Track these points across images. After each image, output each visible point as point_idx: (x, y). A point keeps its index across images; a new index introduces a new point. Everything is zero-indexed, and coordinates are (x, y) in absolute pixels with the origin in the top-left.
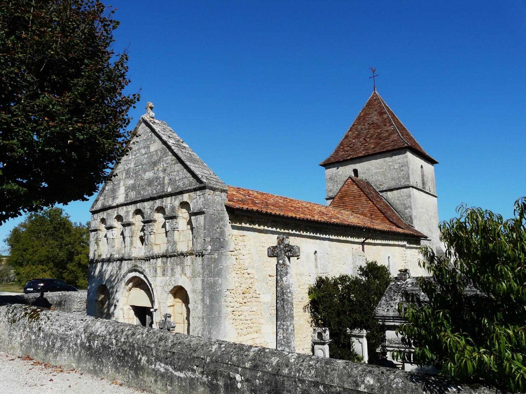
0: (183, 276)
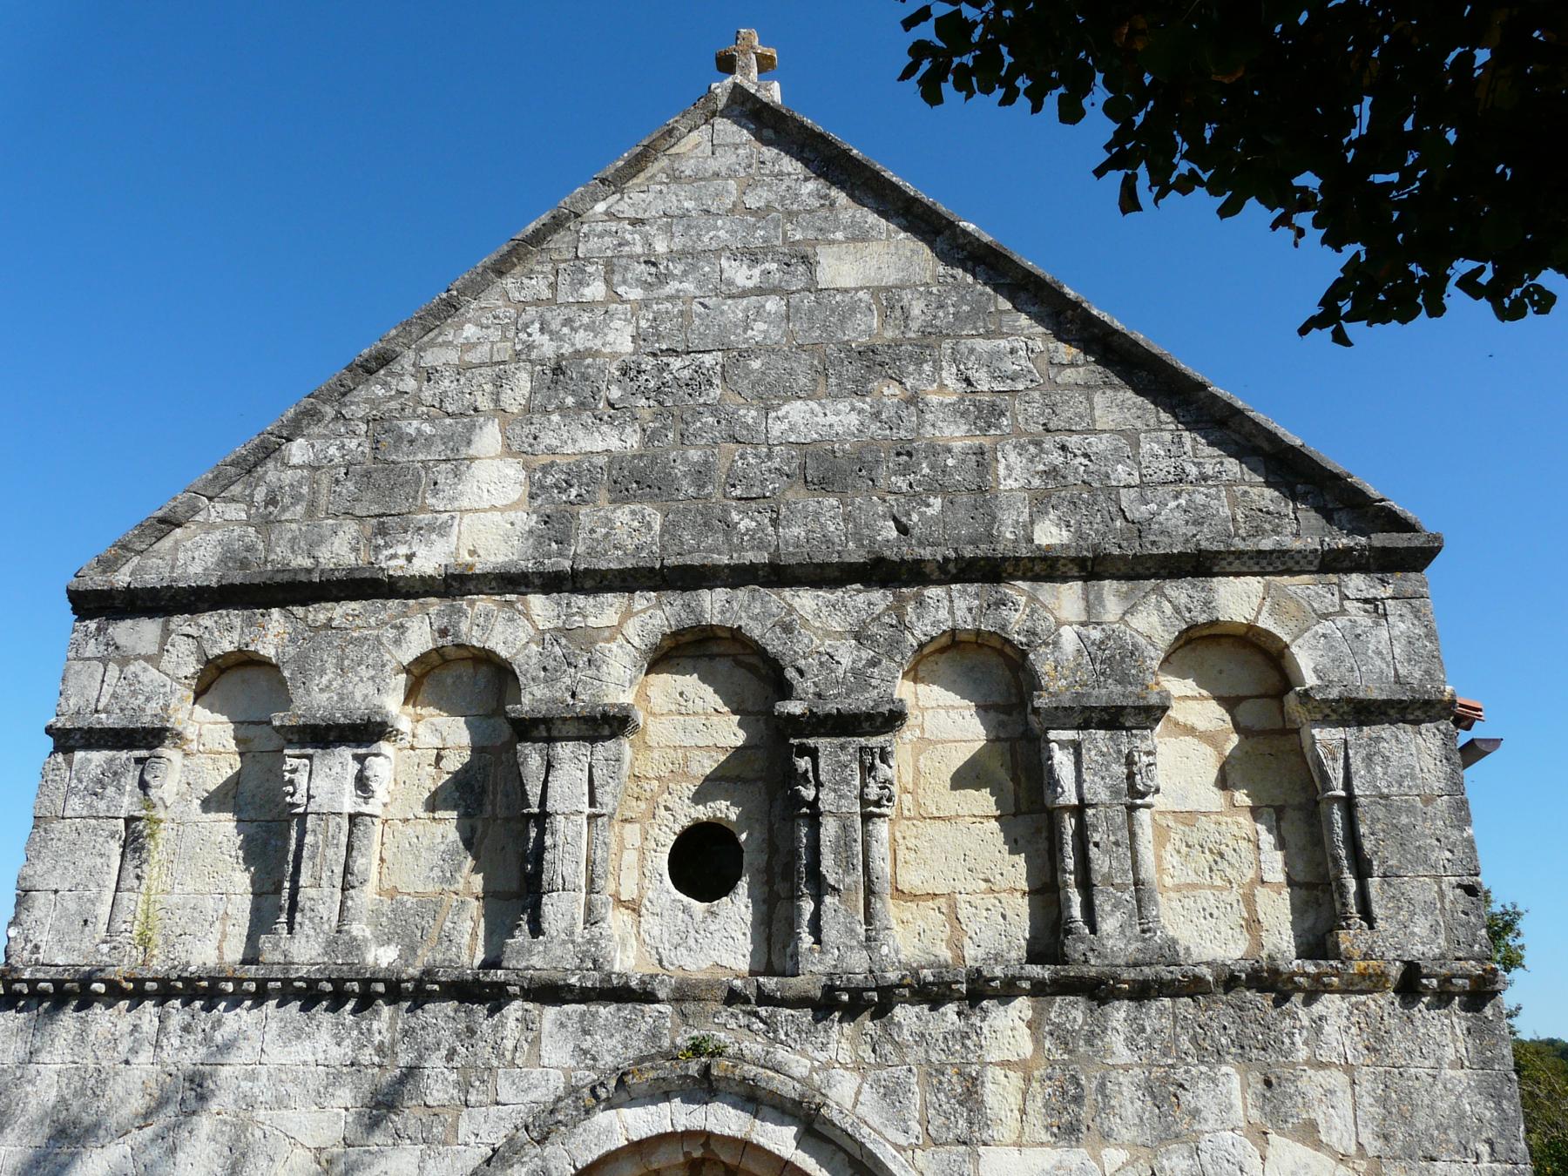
0: (1284, 1150)
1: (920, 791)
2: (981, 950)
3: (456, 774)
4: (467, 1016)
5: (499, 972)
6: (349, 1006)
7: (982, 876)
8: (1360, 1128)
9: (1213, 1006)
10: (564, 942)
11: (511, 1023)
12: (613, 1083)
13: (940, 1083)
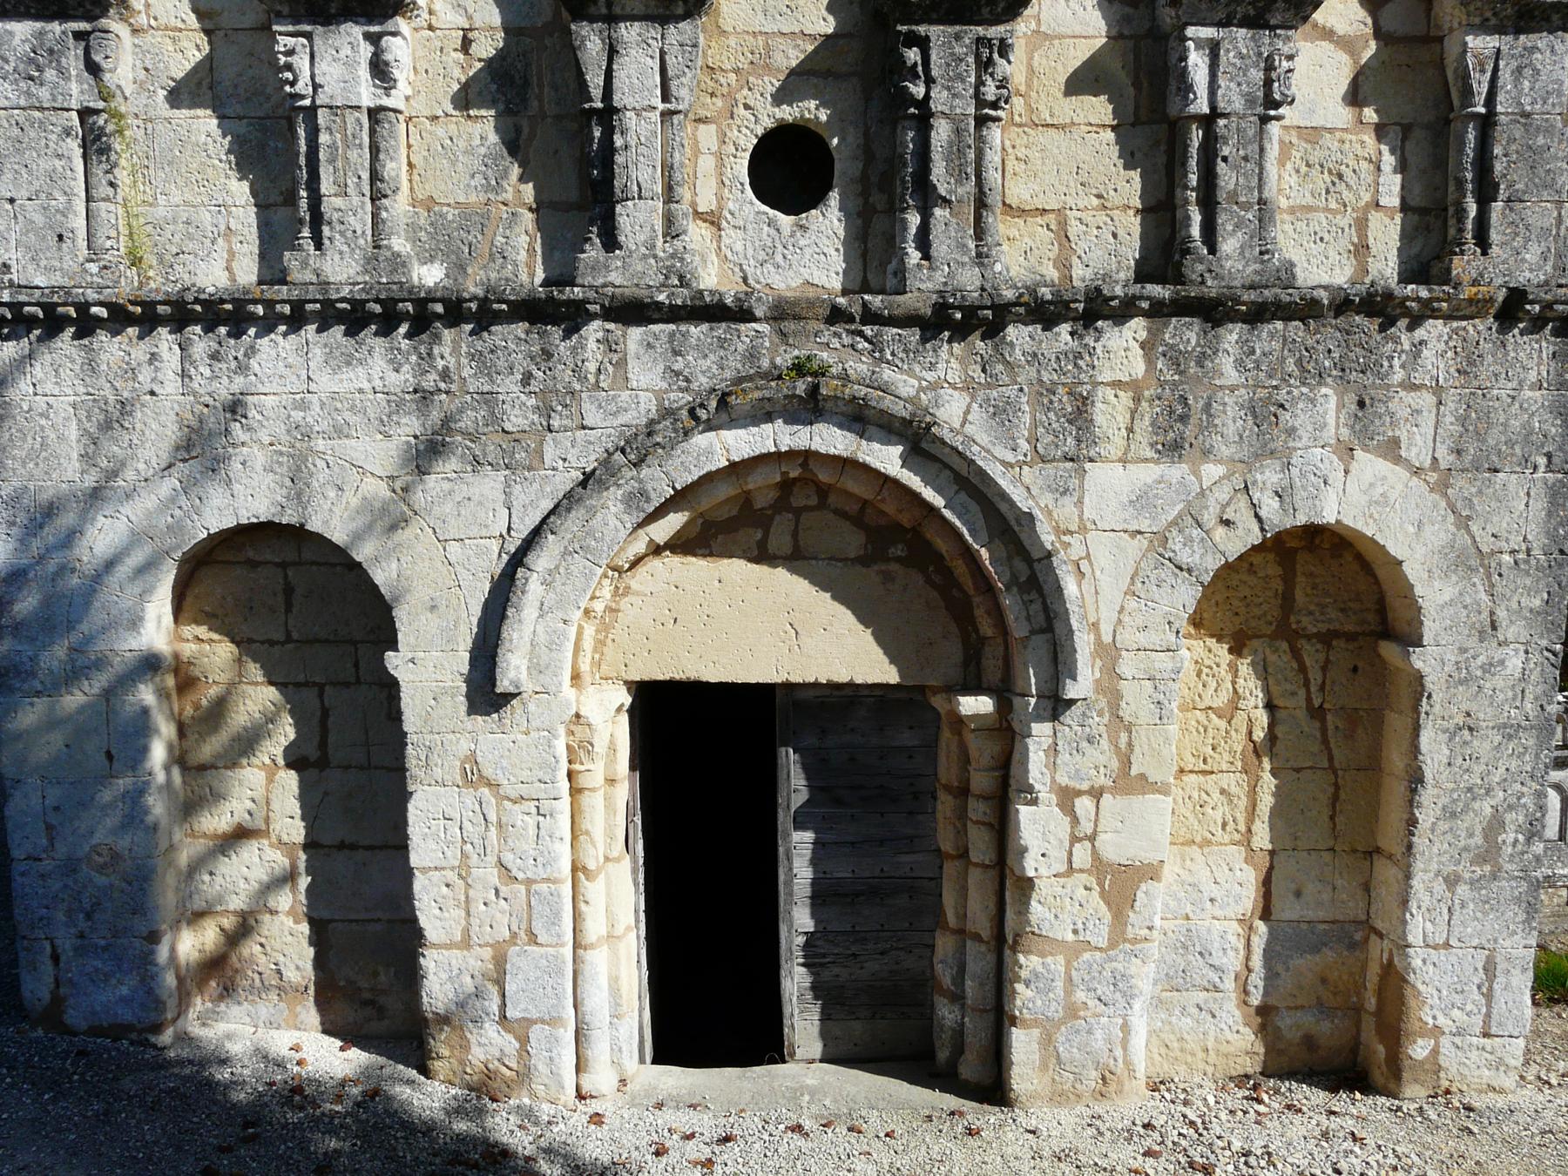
1: (1033, 94)
2: (1090, 270)
3: (489, 62)
6: (403, 329)
7: (1094, 191)
8: (1438, 444)
9: (1322, 329)
10: (645, 257)
11: (592, 345)
12: (714, 404)
13: (1051, 402)
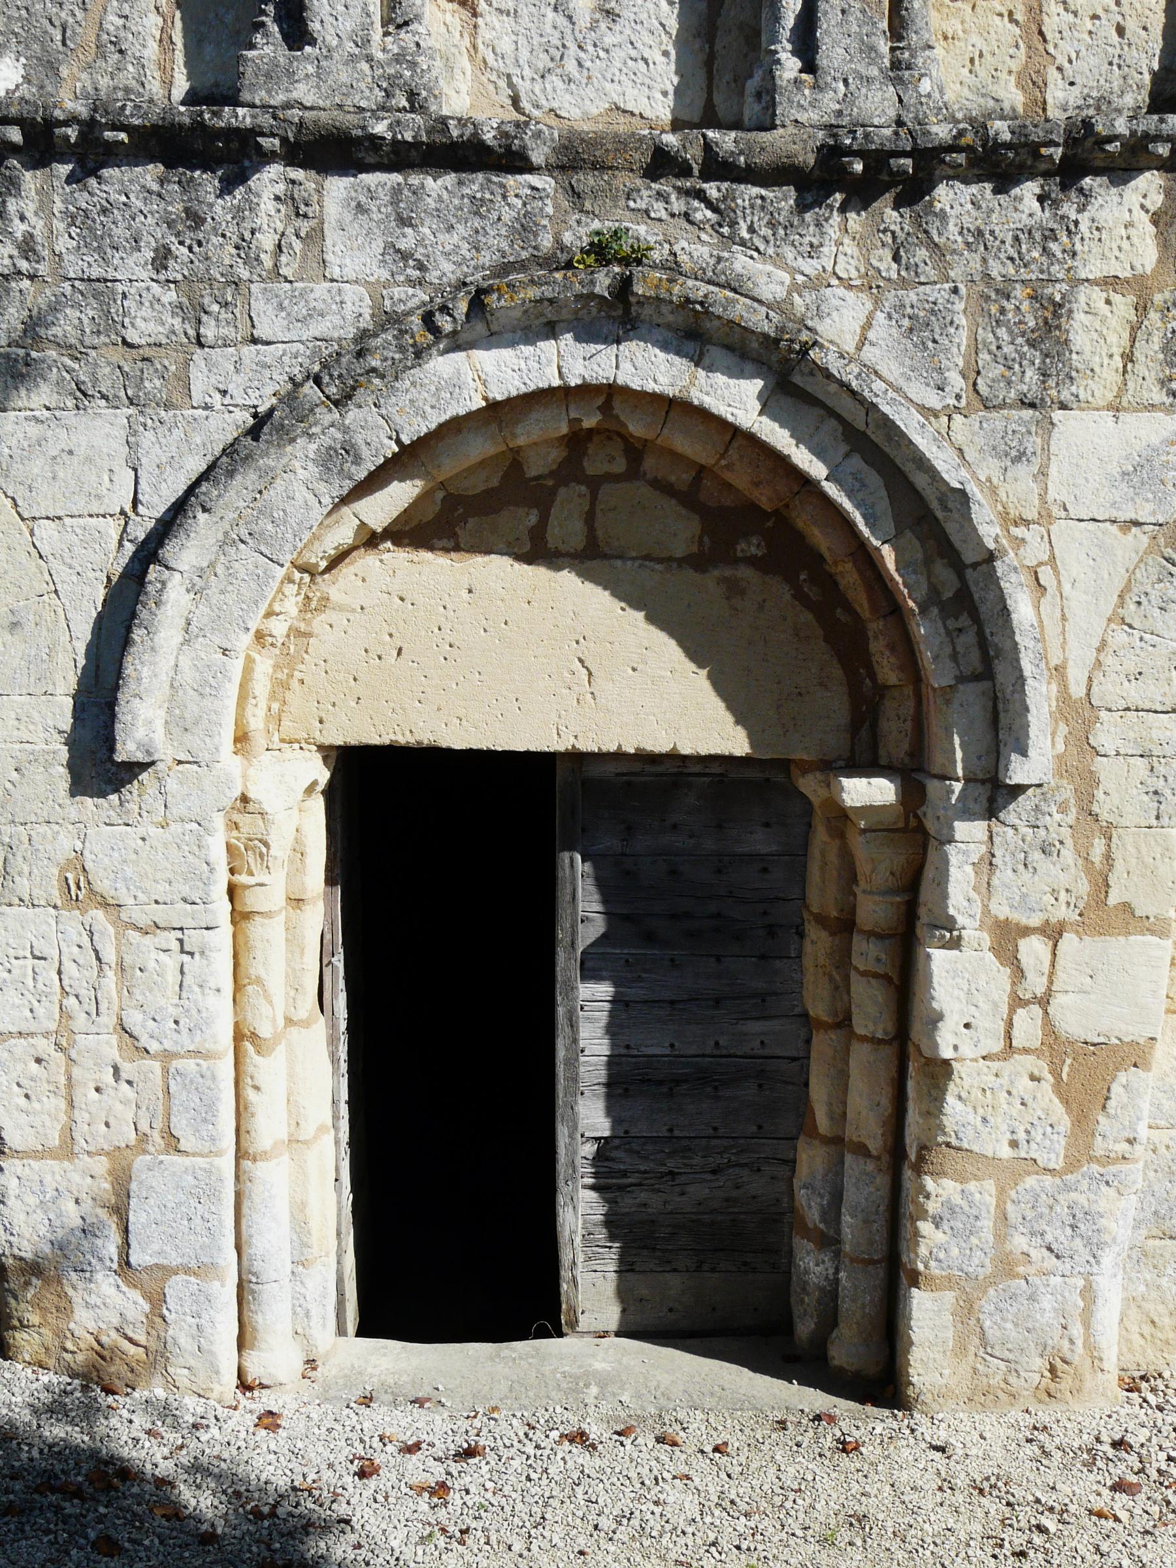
2: (1075, 90)
4: (185, 191)
5: (241, 111)
10: (352, 59)
11: (267, 205)
12: (462, 307)
13: (1003, 311)
